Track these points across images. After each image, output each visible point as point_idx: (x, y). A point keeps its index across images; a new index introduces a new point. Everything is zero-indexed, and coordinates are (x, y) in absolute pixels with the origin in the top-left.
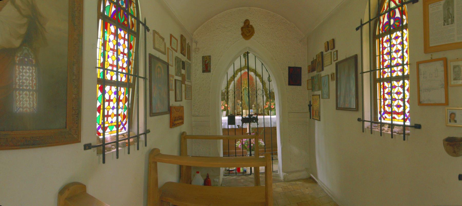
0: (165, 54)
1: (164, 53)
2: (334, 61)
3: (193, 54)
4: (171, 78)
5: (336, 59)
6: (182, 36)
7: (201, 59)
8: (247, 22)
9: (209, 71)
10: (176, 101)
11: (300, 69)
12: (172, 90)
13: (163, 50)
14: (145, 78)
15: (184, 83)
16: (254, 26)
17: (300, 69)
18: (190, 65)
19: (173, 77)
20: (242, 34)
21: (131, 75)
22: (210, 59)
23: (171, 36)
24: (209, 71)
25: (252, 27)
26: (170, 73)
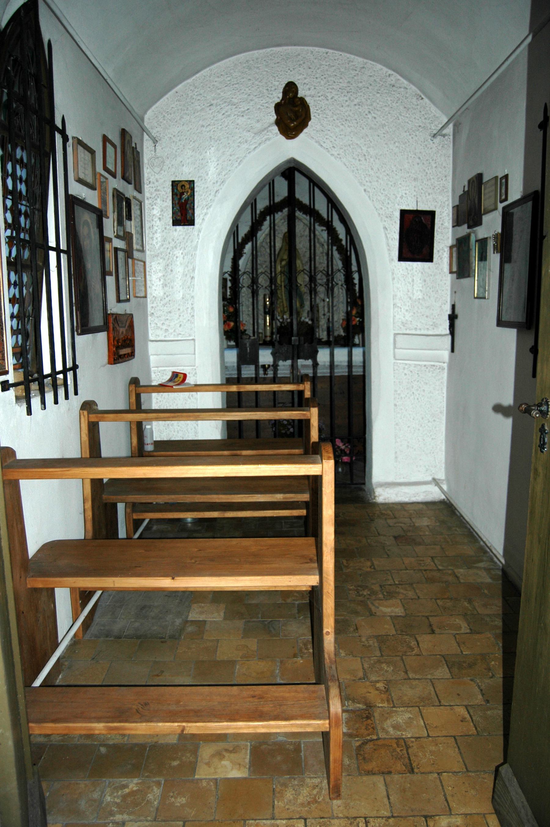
0: (94, 189)
1: (92, 187)
2: (501, 202)
3: (147, 173)
4: (107, 246)
5: (503, 197)
6: (124, 133)
7: (169, 190)
8: (290, 88)
9: (191, 223)
10: (119, 301)
11: (431, 214)
12: (110, 274)
13: (89, 180)
14: (57, 249)
15: (132, 258)
16: (308, 99)
17: (431, 214)
18: (141, 204)
19: (110, 240)
20: (278, 123)
21: (52, 249)
22: (193, 189)
23: (105, 139)
24: (191, 223)
25: (302, 101)
26: (105, 234)
